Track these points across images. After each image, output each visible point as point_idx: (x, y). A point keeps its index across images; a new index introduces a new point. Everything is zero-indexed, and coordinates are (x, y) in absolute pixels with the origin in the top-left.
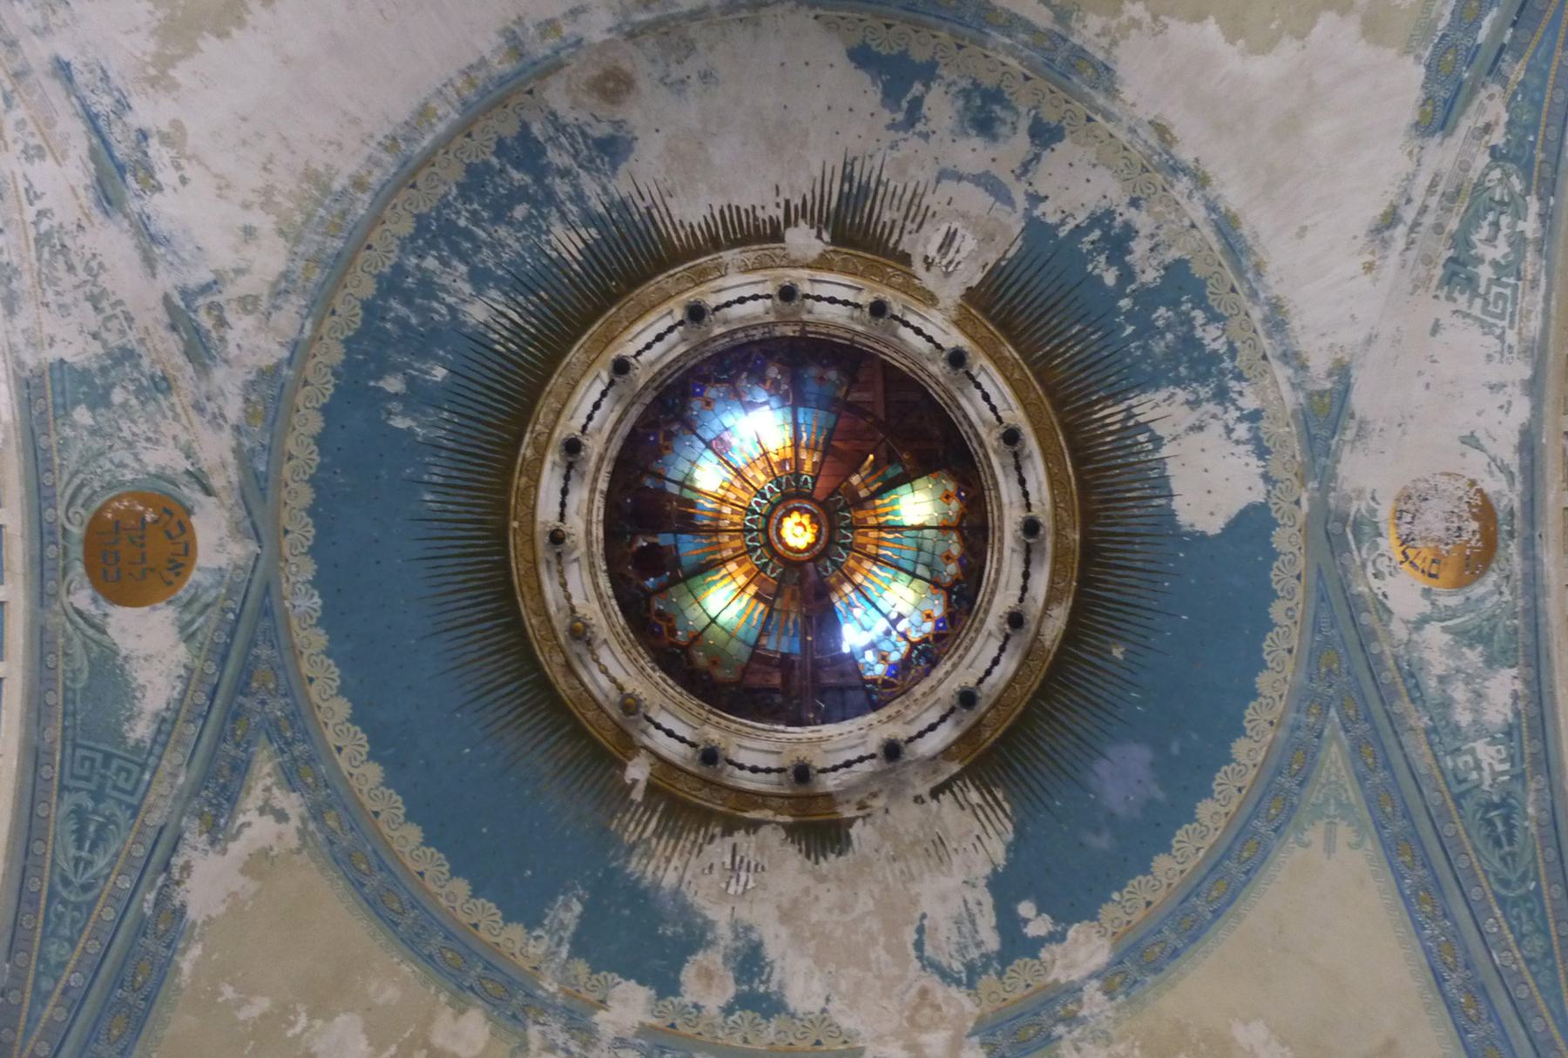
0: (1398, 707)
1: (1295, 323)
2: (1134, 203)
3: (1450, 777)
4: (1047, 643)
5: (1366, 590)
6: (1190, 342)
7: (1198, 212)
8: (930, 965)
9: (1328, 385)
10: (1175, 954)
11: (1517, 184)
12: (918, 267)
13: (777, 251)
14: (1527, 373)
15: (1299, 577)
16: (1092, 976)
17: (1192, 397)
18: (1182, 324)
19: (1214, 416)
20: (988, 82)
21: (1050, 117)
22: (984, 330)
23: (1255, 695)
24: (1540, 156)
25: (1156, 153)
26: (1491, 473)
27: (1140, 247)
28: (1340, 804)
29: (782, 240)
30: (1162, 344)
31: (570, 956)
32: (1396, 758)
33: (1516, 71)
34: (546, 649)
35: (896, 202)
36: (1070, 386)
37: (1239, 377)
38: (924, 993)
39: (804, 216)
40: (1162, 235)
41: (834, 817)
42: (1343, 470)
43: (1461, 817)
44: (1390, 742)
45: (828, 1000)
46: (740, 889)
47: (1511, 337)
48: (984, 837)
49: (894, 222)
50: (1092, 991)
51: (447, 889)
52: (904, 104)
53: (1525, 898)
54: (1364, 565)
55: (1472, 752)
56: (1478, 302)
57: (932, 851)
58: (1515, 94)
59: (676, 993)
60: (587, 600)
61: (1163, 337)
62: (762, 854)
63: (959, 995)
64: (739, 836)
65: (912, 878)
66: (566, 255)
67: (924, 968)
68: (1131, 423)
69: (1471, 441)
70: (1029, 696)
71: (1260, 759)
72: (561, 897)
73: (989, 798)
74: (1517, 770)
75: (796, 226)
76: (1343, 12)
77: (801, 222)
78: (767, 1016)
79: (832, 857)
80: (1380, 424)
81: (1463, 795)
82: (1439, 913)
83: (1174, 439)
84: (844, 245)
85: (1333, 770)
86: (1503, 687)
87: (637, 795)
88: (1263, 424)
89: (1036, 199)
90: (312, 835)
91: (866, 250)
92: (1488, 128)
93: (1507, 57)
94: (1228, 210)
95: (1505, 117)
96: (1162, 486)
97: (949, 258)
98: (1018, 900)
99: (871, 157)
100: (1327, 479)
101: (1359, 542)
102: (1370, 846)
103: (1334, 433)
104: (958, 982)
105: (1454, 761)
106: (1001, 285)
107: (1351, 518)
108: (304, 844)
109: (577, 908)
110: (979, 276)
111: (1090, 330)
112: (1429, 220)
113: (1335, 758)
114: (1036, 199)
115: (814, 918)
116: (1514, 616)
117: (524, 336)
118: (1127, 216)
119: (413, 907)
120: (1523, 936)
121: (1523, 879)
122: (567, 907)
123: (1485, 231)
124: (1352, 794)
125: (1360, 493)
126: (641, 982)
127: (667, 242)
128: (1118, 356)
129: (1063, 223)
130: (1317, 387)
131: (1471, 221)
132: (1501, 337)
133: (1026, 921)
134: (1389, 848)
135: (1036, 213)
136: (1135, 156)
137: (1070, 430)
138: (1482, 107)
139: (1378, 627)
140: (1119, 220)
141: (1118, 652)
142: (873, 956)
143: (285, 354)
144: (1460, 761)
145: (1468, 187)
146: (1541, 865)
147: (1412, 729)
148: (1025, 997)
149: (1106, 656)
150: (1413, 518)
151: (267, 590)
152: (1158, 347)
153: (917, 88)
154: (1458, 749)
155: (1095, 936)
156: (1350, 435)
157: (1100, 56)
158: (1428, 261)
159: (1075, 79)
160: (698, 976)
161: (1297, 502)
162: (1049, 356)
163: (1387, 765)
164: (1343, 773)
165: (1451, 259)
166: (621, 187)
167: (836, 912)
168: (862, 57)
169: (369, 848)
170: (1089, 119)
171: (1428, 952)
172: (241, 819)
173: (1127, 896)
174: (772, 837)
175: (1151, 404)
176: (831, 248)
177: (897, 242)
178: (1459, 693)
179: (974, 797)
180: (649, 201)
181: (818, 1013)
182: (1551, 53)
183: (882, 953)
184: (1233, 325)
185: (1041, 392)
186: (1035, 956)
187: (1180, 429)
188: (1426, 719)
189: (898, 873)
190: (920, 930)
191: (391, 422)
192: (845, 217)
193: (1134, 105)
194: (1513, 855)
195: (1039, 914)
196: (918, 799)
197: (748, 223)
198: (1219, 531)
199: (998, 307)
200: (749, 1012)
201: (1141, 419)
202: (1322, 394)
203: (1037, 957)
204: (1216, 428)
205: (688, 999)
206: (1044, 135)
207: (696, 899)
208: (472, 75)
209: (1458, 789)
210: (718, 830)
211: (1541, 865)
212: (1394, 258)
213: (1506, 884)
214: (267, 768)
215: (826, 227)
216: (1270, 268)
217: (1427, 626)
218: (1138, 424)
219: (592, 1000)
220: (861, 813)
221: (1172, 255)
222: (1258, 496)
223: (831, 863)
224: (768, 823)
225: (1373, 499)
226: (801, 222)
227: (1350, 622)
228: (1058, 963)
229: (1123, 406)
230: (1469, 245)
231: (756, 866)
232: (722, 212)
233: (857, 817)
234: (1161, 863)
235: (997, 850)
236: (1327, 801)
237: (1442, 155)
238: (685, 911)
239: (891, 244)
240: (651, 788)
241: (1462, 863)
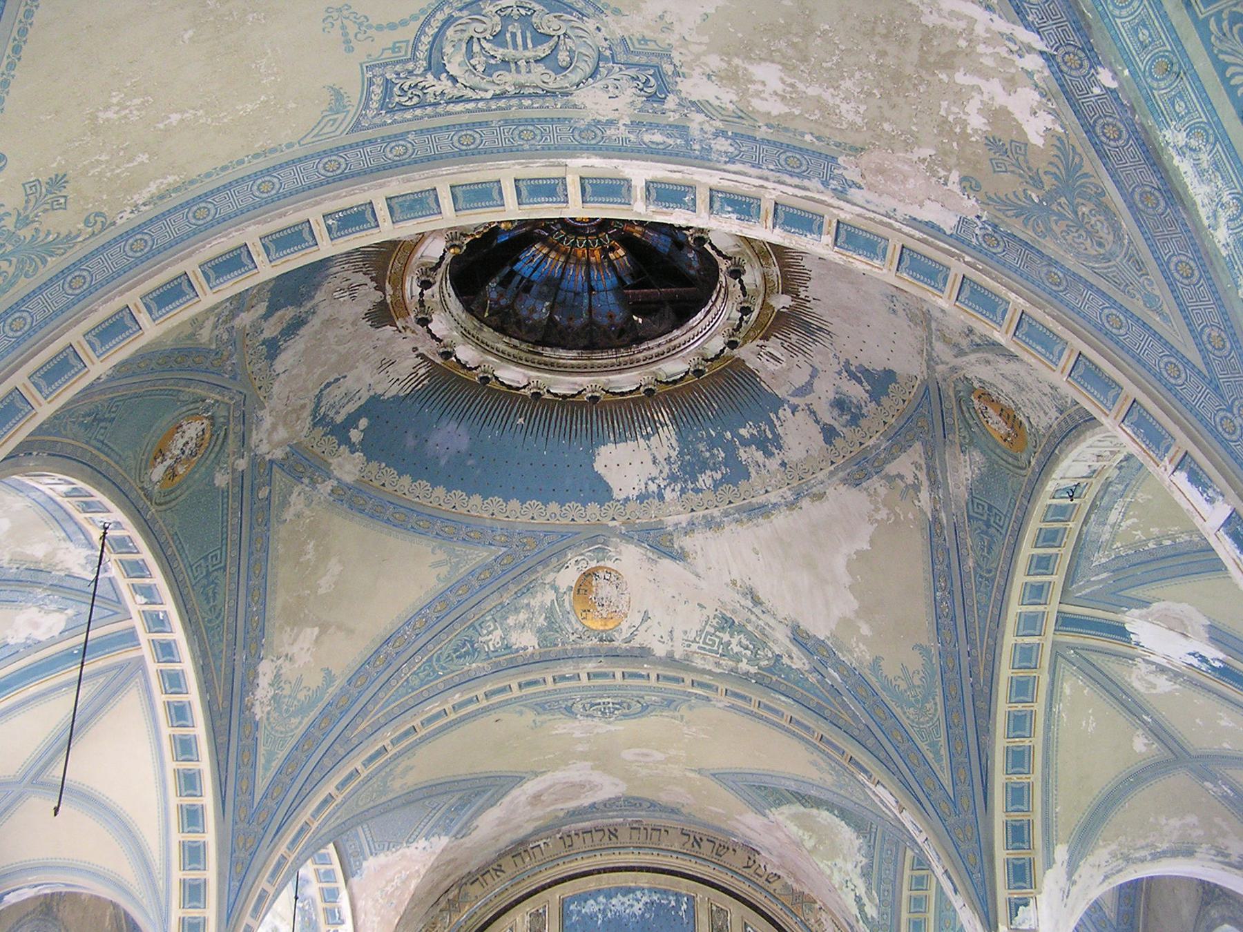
0: (511, 586)
1: (709, 534)
2: (783, 464)
3: (481, 620)
6: (704, 465)
7: (773, 497)
8: (319, 398)
10: (362, 511)
11: (764, 663)
14: (677, 657)
18: (714, 463)
19: (661, 472)
20: (862, 422)
21: (838, 442)
23: (506, 500)
24: (774, 678)
26: (630, 627)
27: (759, 455)
28: (458, 563)
33: (813, 678)
37: (683, 491)
38: (303, 407)
40: (764, 472)
42: (631, 547)
44: (494, 587)
47: (694, 647)
50: (330, 484)
52: (859, 375)
53: (434, 671)
54: (582, 554)
55: (496, 628)
56: (712, 631)
58: (802, 674)
63: (308, 422)
68: (658, 425)
69: (646, 617)
71: (472, 513)
74: (491, 655)
76: (856, 612)
81: (475, 628)
82: (417, 631)
86: (527, 640)
88: (656, 501)
89: (794, 409)
92: (790, 657)
93: (820, 677)
95: (794, 667)
96: (620, 439)
101: (593, 551)
104: (315, 417)
112: (753, 618)
113: (481, 555)
114: (794, 409)
116: (563, 643)
120: (417, 674)
121: (443, 668)
123: (745, 642)
124: (463, 570)
128: (698, 424)
129: (778, 418)
130: (675, 539)
131: (749, 635)
132: (694, 641)
133: (357, 427)
134: (441, 597)
135: (786, 406)
138: (801, 659)
139: (551, 567)
140: (776, 452)
145: (767, 640)
146: (451, 675)
152: (702, 447)
156: (650, 554)
157: (864, 484)
158: (734, 611)
161: (614, 519)
162: (700, 391)
163: (482, 587)
165: (734, 622)
170: (832, 463)
171: (398, 631)
178: (523, 616)
182: (817, 696)
184: (711, 496)
187: (654, 451)
190: (337, 380)
194: (452, 659)
201: (660, 430)
202: (671, 541)
203: (339, 446)
204: (655, 473)
206: (829, 433)
211: (451, 675)
212: (738, 597)
213: (438, 660)
216: (739, 528)
221: (752, 471)
222: (617, 494)
228: (340, 459)
229: (668, 422)
230: (739, 633)
236: (457, 556)
237: (781, 641)
241: (443, 636)
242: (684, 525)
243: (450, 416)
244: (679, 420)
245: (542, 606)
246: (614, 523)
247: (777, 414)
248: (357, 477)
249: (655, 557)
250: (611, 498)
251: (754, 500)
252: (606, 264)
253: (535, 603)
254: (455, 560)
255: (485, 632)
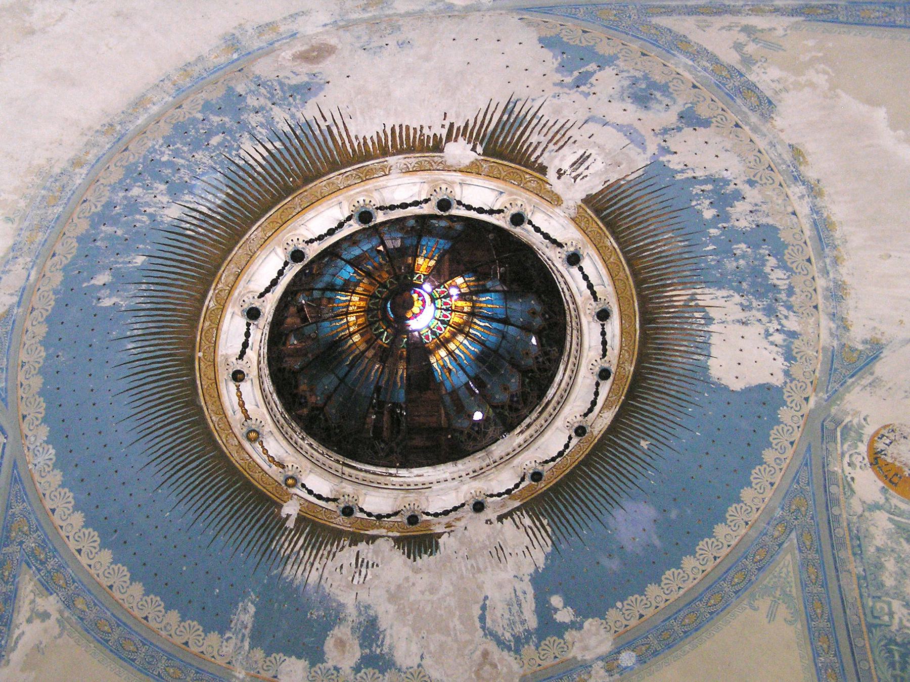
1: (850, 302)
3: (868, 611)
4: (595, 433)
5: (840, 471)
7: (803, 209)
8: (490, 633)
9: (860, 347)
12: (551, 176)
13: (436, 159)
15: (792, 443)
16: (599, 658)
17: (746, 303)
22: (595, 225)
25: (785, 163)
28: (784, 592)
29: (442, 151)
30: (735, 264)
31: (252, 647)
32: (833, 585)
34: (223, 436)
35: (545, 130)
36: (653, 271)
37: (790, 308)
38: (485, 654)
39: (464, 134)
41: (429, 532)
42: (849, 397)
43: (869, 638)
45: (422, 657)
46: (362, 580)
48: (531, 548)
49: (539, 143)
51: (165, 622)
54: (843, 454)
55: (889, 604)
57: (494, 554)
59: (323, 661)
60: (257, 406)
61: (737, 260)
62: (377, 556)
63: (508, 657)
64: (362, 546)
65: (479, 570)
66: (252, 162)
67: (485, 635)
70: (576, 463)
72: (240, 604)
73: (538, 523)
75: (456, 141)
77: (460, 138)
78: (382, 671)
79: (425, 556)
80: (873, 333)
81: (875, 626)
83: (723, 322)
84: (492, 156)
85: (784, 570)
87: (290, 524)
88: (797, 343)
90: (68, 620)
91: (511, 161)
94: (828, 217)
97: (579, 172)
98: (552, 593)
99: (533, 100)
100: (834, 397)
101: (844, 440)
102: (799, 626)
103: (852, 376)
104: (509, 649)
105: (874, 603)
106: (616, 196)
107: (844, 424)
108: (63, 628)
109: (252, 609)
110: (601, 188)
111: (679, 239)
115: (412, 598)
117: (211, 222)
118: (740, 186)
119: (144, 644)
122: (245, 610)
125: (856, 413)
126: (299, 657)
127: (342, 150)
129: (682, 171)
130: (851, 344)
134: (812, 634)
136: (766, 158)
137: (644, 300)
139: (842, 498)
141: (644, 444)
142: (451, 625)
143: (15, 299)
144: (879, 605)
147: (849, 571)
148: (553, 666)
149: (637, 446)
150: (891, 443)
151: (15, 466)
152: (730, 265)
153: (592, 67)
154: (879, 598)
155: (602, 631)
156: (864, 382)
159: (739, 101)
160: (335, 645)
161: (807, 399)
164: (791, 574)
166: (309, 112)
167: (427, 593)
168: (546, 42)
169: (109, 613)
172: (17, 632)
173: (627, 607)
174: (385, 546)
175: (712, 296)
176: (482, 158)
177: (538, 157)
179: (527, 521)
180: (330, 121)
181: (416, 667)
183: (457, 622)
185: (628, 272)
186: (561, 636)
187: (730, 319)
188: (861, 569)
189: (469, 567)
190: (484, 608)
191: (102, 305)
192: (499, 137)
193: (782, 131)
195: (565, 606)
196: (488, 522)
197: (414, 137)
198: (739, 390)
199: (608, 211)
200: (370, 669)
202: (853, 350)
205: (330, 664)
207: (333, 590)
208: (189, 69)
209: (870, 619)
210: (347, 543)
214: (30, 587)
215: (481, 143)
217: (878, 511)
218: (697, 305)
219: (268, 677)
220: (447, 530)
221: (763, 220)
222: (778, 380)
223: (425, 560)
224: (383, 536)
225: (865, 419)
226: (460, 138)
227: (822, 489)
229: (690, 292)
231: (373, 565)
232: (393, 129)
233: (445, 532)
234: (652, 590)
235: (539, 557)
238: (325, 599)
239: (533, 159)
240: (301, 519)
241: (863, 665)
242: (833, 326)
243: (603, 511)
244: (687, 280)
245: (890, 536)
246: (812, 401)
247: (677, 172)
248: (611, 639)
249: (869, 379)
250: (779, 390)
251: (807, 233)
252: (474, 298)
253: (880, 540)
254: (778, 593)
255: (886, 618)
